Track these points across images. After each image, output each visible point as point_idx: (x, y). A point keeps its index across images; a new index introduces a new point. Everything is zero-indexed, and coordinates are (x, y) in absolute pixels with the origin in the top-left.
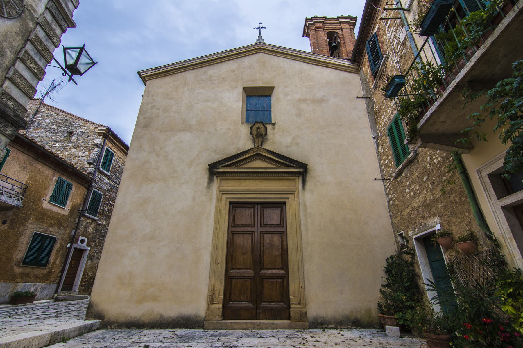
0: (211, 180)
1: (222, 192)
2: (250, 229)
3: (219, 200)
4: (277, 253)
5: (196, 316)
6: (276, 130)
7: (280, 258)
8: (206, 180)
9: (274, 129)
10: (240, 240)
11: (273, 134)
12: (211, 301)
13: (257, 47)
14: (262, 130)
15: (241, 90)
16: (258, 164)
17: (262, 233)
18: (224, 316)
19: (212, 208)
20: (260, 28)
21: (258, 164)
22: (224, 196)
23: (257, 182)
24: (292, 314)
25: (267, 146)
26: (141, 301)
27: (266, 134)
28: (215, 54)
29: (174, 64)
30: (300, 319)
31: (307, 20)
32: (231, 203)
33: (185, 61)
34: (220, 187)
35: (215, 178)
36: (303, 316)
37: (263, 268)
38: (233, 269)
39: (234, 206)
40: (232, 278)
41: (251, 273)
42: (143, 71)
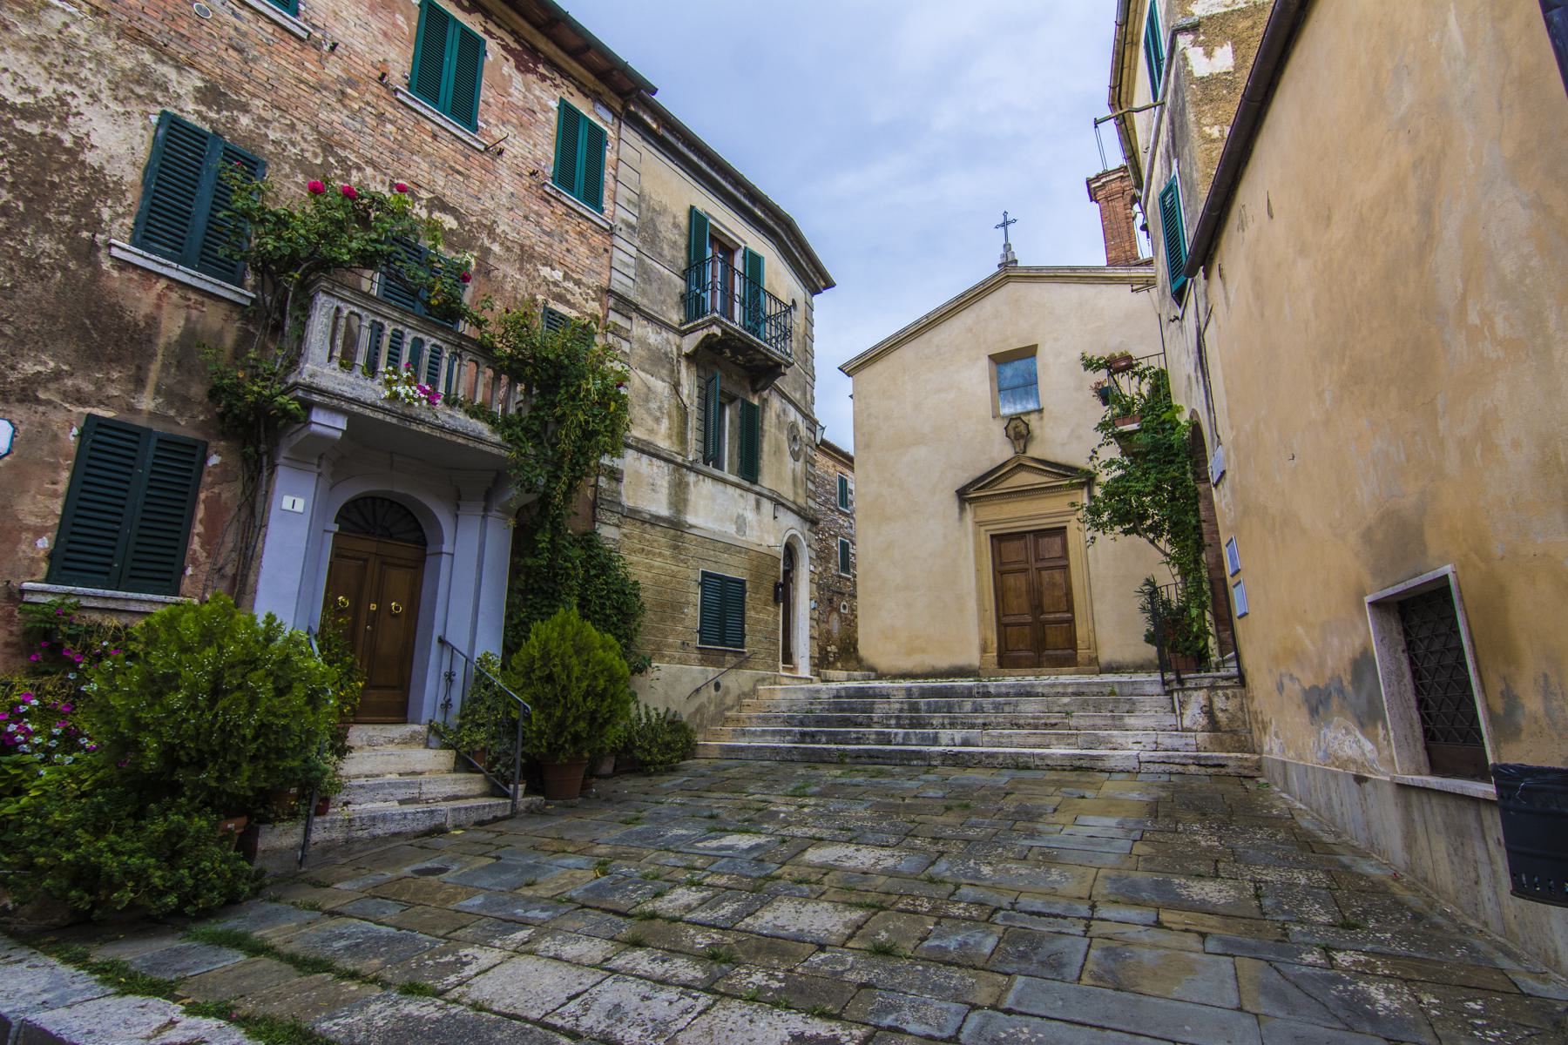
0: (962, 510)
1: (979, 524)
2: (1022, 566)
3: (976, 534)
4: (1058, 593)
5: (970, 666)
6: (1045, 419)
7: (1064, 599)
8: (956, 510)
9: (1042, 418)
10: (1011, 580)
11: (1041, 428)
12: (984, 649)
13: (1003, 275)
14: (1022, 429)
15: (985, 362)
16: (1024, 479)
17: (1039, 570)
18: (1001, 665)
19: (969, 545)
20: (1005, 224)
21: (1024, 479)
22: (983, 529)
23: (1024, 503)
24: (1079, 659)
25: (1034, 451)
26: (910, 652)
27: (1029, 432)
28: (938, 309)
29: (883, 343)
30: (1090, 664)
31: (1089, 182)
32: (992, 536)
33: (897, 334)
34: (975, 516)
35: (967, 505)
36: (1094, 661)
37: (1043, 613)
38: (1005, 615)
39: (998, 539)
40: (1006, 625)
41: (1029, 619)
42: (845, 365)
